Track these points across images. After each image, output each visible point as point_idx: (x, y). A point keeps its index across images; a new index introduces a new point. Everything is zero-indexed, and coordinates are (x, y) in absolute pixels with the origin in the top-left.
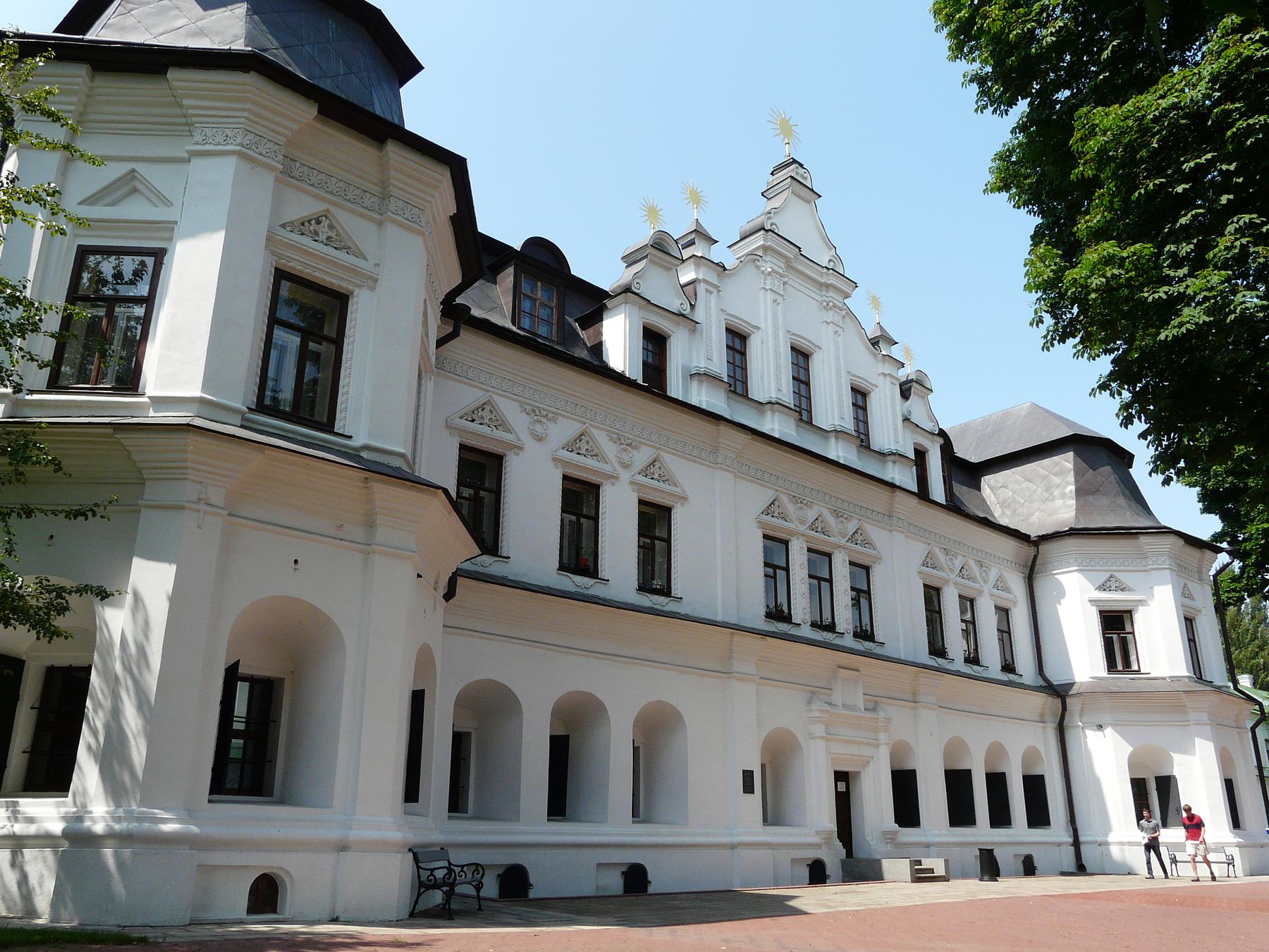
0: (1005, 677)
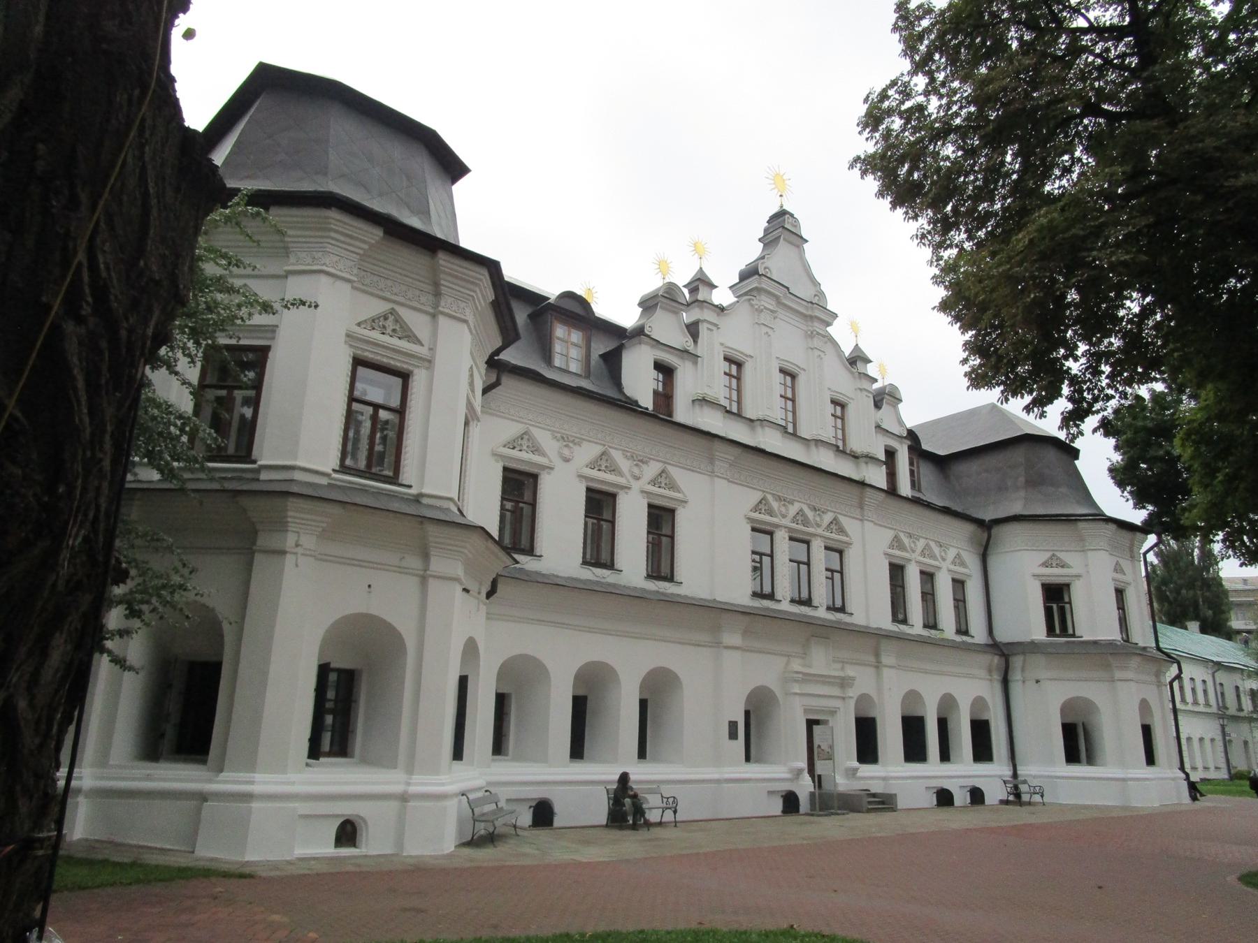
0: (959, 638)
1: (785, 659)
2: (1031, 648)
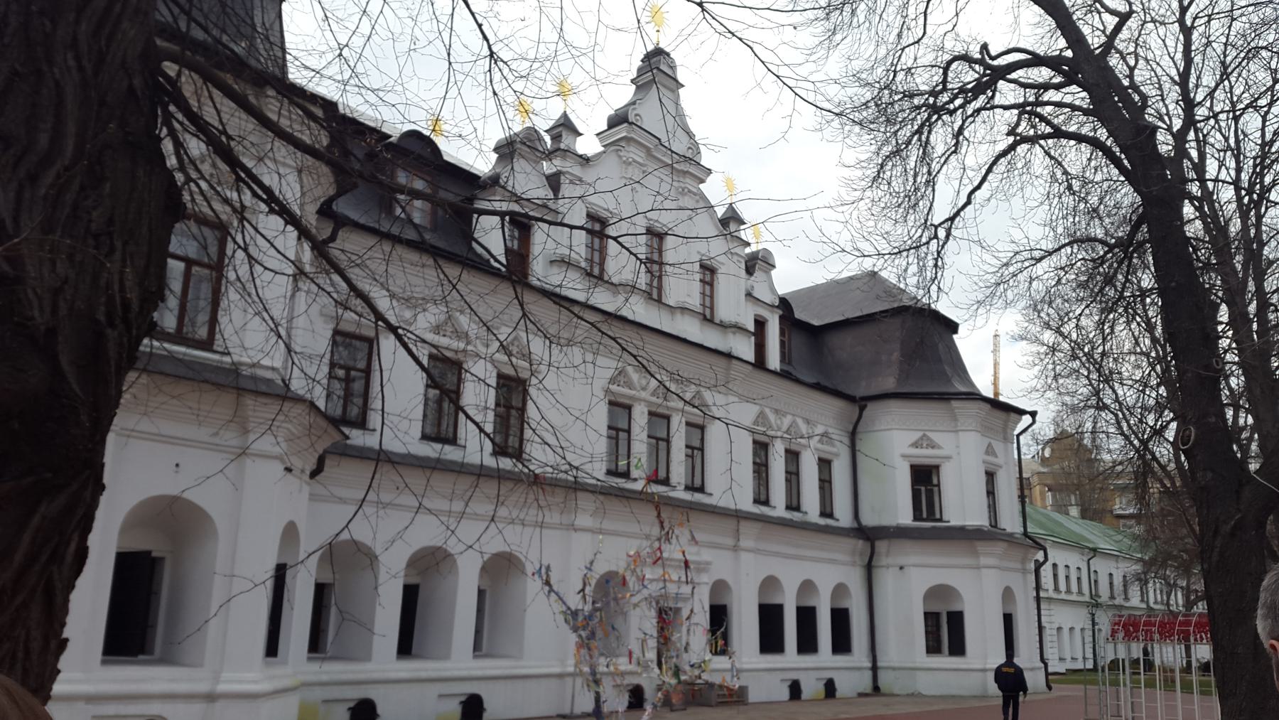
2: (899, 533)
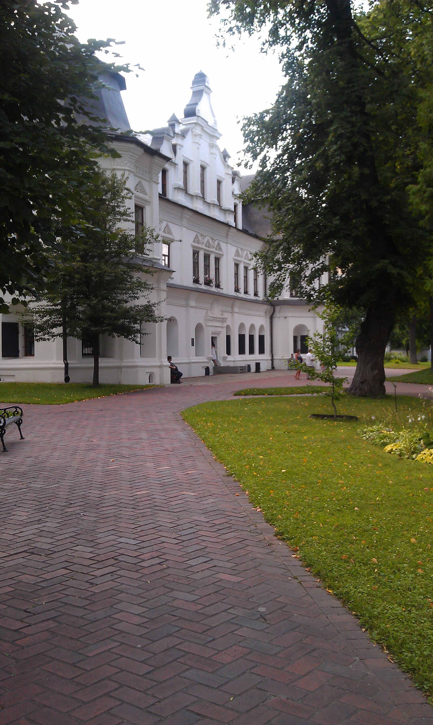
1: (205, 311)
